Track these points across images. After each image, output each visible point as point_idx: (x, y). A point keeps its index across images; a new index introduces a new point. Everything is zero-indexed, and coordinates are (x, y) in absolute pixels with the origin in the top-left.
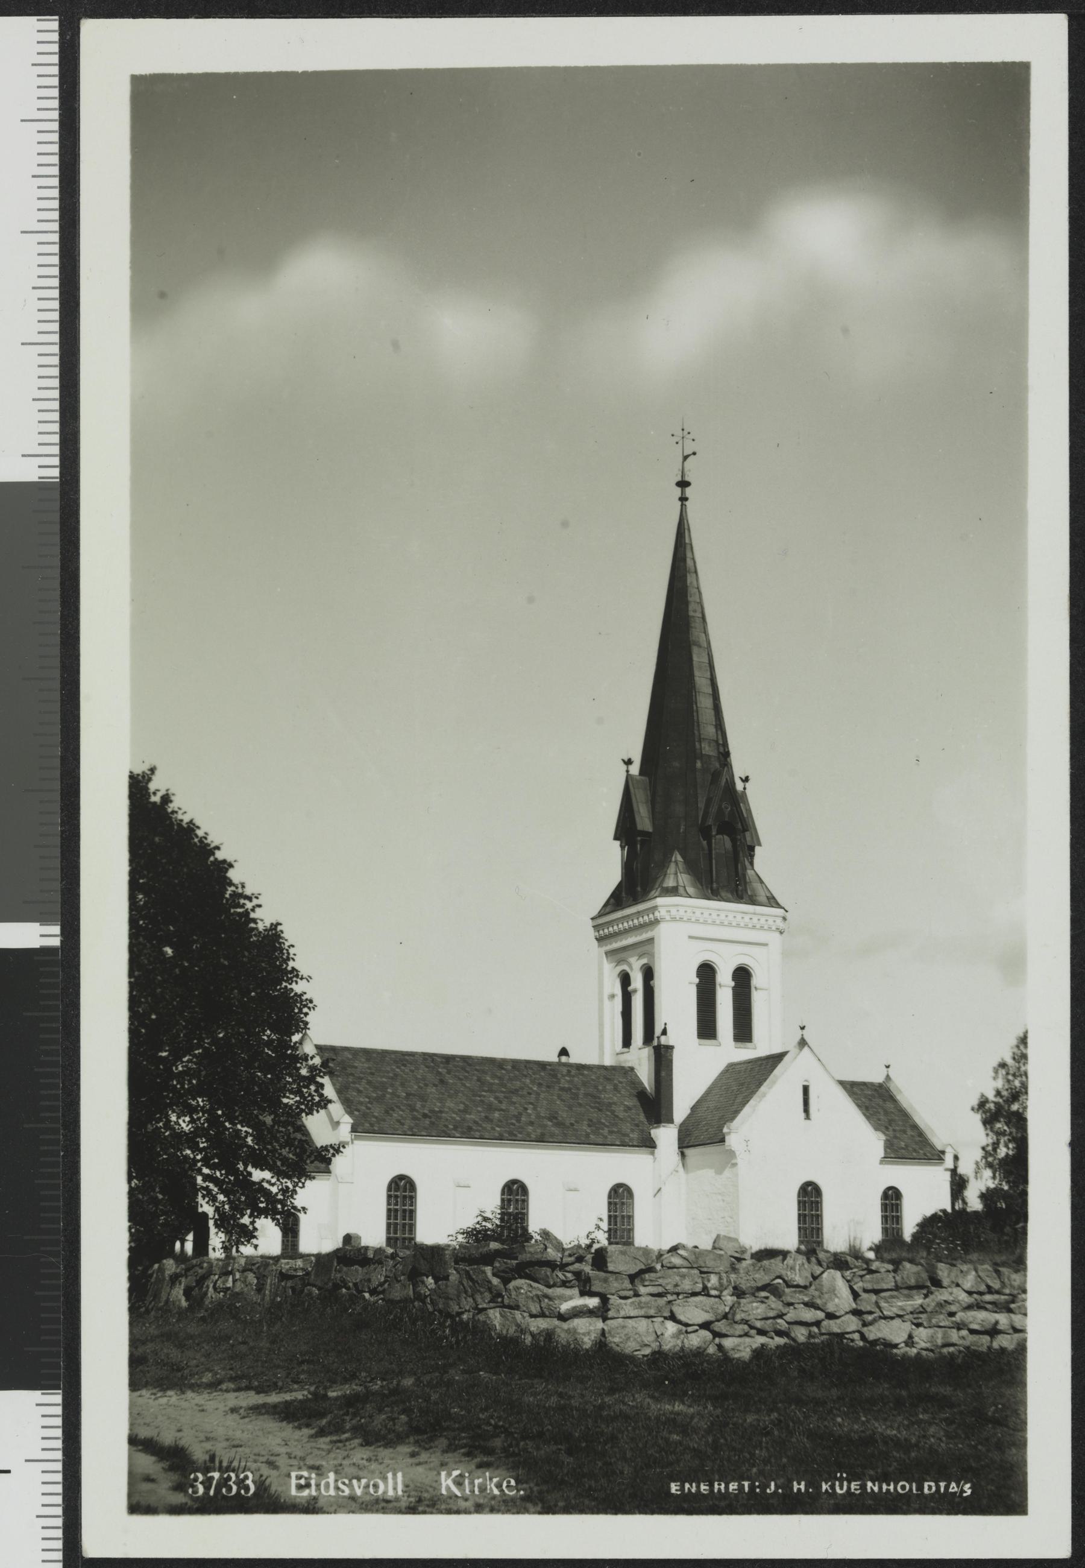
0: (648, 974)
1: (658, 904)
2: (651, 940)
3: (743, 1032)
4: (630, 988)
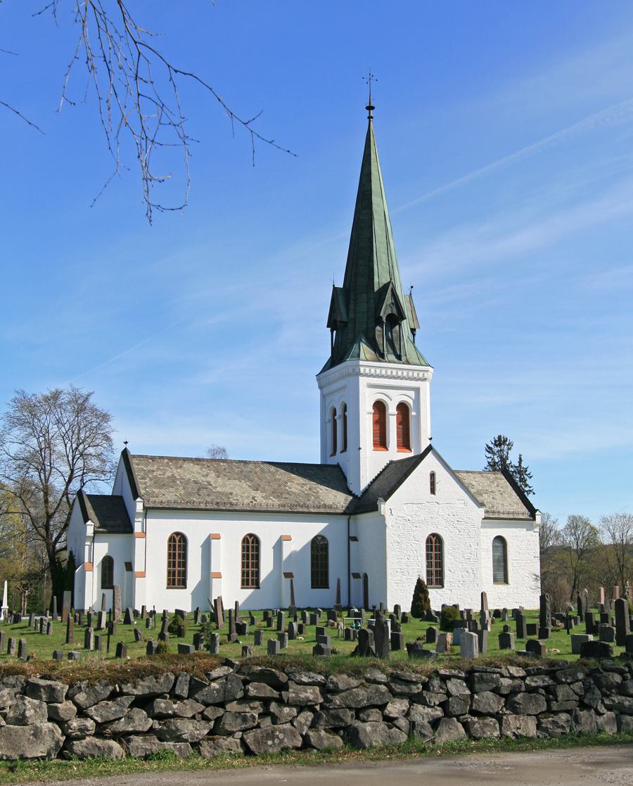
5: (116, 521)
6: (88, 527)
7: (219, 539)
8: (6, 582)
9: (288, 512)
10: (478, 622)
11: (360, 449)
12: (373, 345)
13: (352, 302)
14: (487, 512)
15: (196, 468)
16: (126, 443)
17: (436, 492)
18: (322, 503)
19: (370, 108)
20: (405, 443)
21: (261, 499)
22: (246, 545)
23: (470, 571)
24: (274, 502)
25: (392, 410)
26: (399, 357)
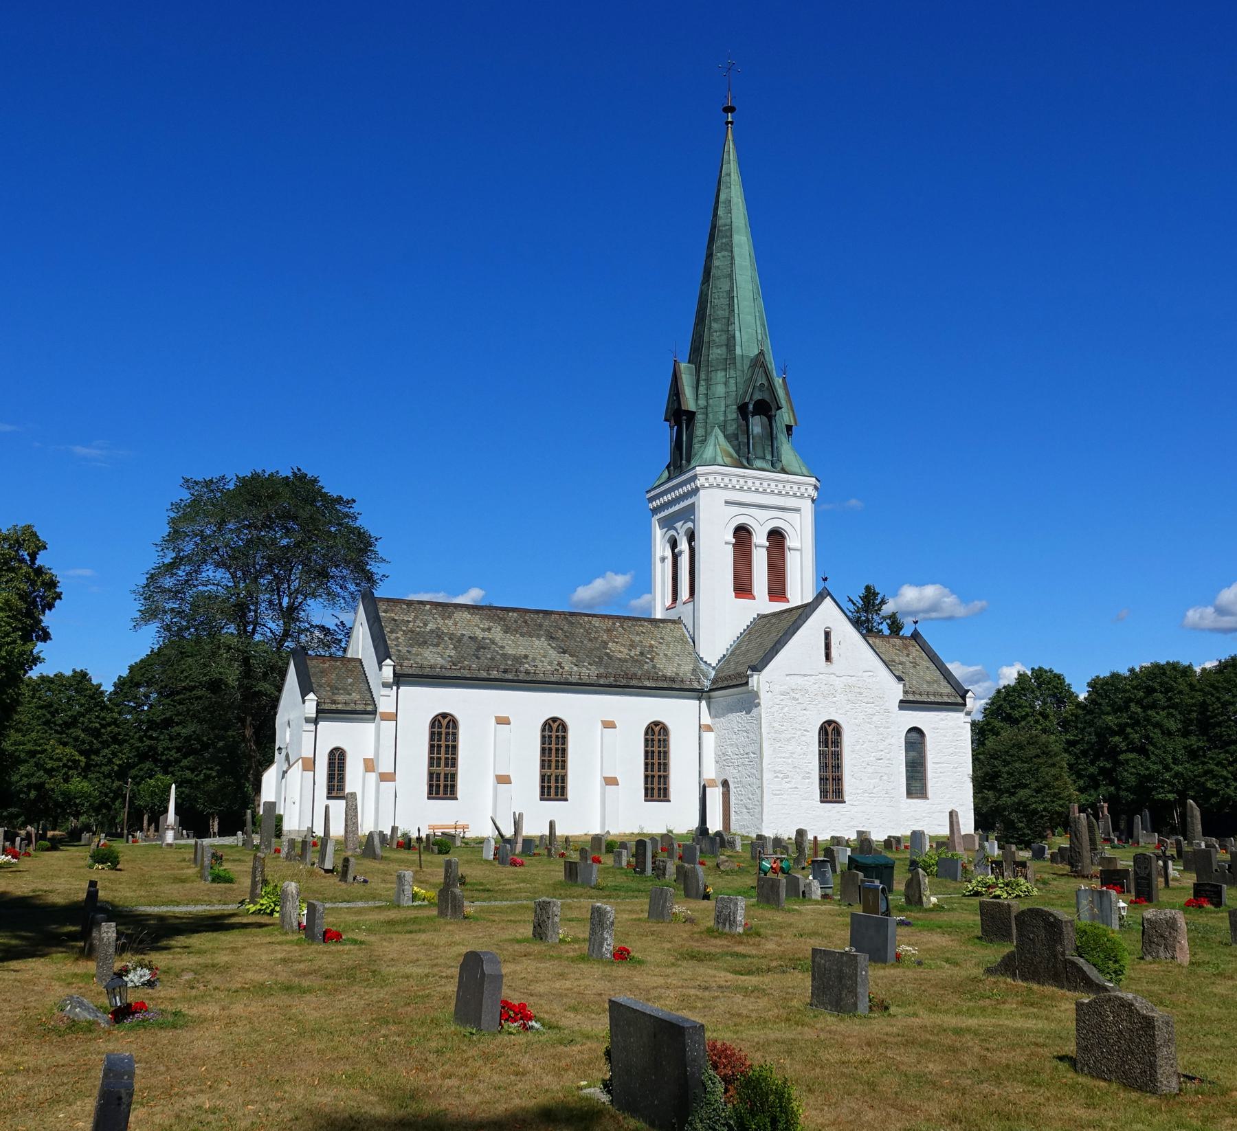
0: (691, 537)
1: (697, 472)
2: (693, 504)
3: (777, 590)
4: (676, 551)
5: (350, 695)
7: (509, 724)
8: (173, 786)
10: (33, 836)
13: (702, 383)
14: (905, 692)
18: (660, 673)
20: (777, 590)
24: (589, 672)
25: (760, 539)
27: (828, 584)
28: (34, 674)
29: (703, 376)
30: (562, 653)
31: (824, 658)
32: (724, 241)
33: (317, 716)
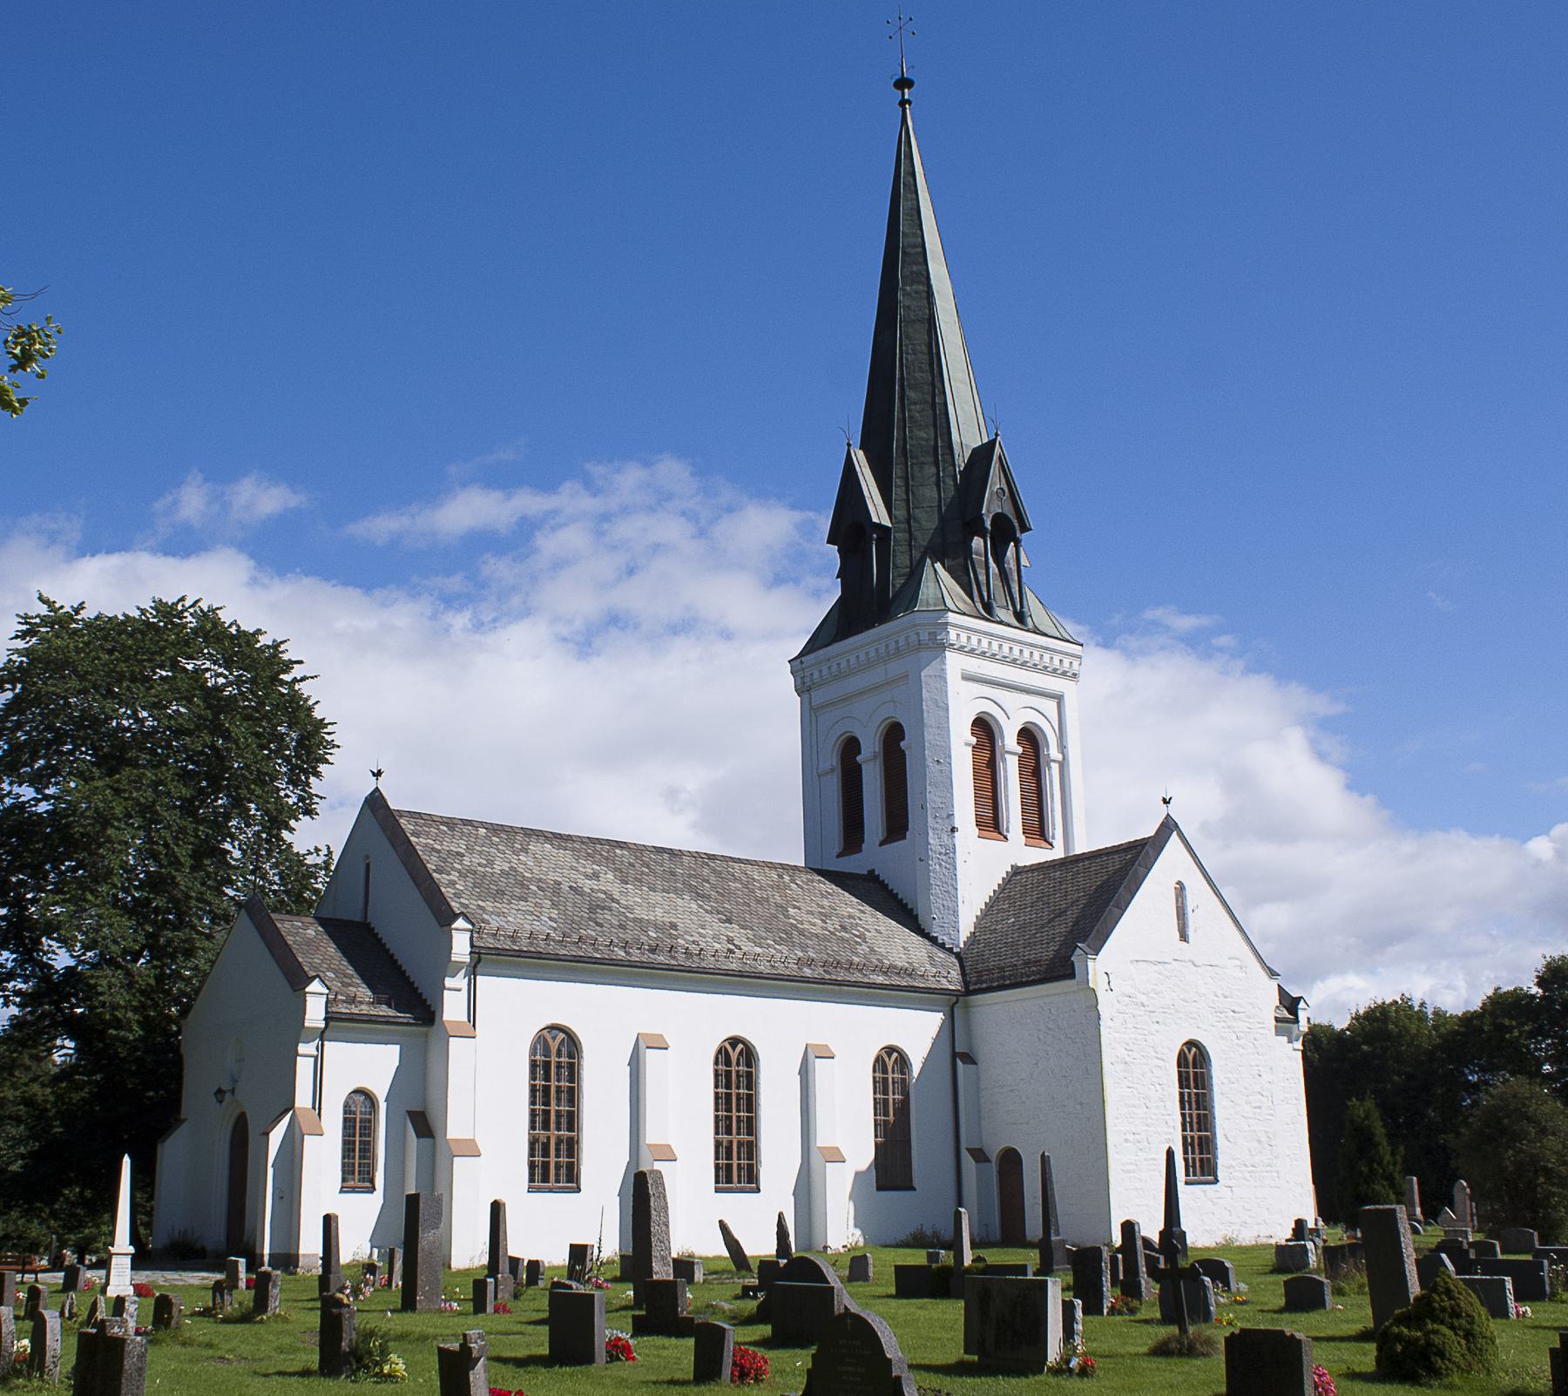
3: (1037, 830)
6: (309, 998)
9: (822, 982)
11: (953, 830)
12: (963, 576)
15: (565, 857)
16: (378, 774)
17: (1191, 939)
19: (903, 83)
21: (750, 948)
22: (539, 1083)
23: (1264, 1139)
25: (1010, 739)
26: (1020, 617)
27: (1175, 811)
28: (258, 646)
29: (897, 471)
30: (725, 922)
31: (1177, 935)
32: (915, 268)
33: (327, 1025)
